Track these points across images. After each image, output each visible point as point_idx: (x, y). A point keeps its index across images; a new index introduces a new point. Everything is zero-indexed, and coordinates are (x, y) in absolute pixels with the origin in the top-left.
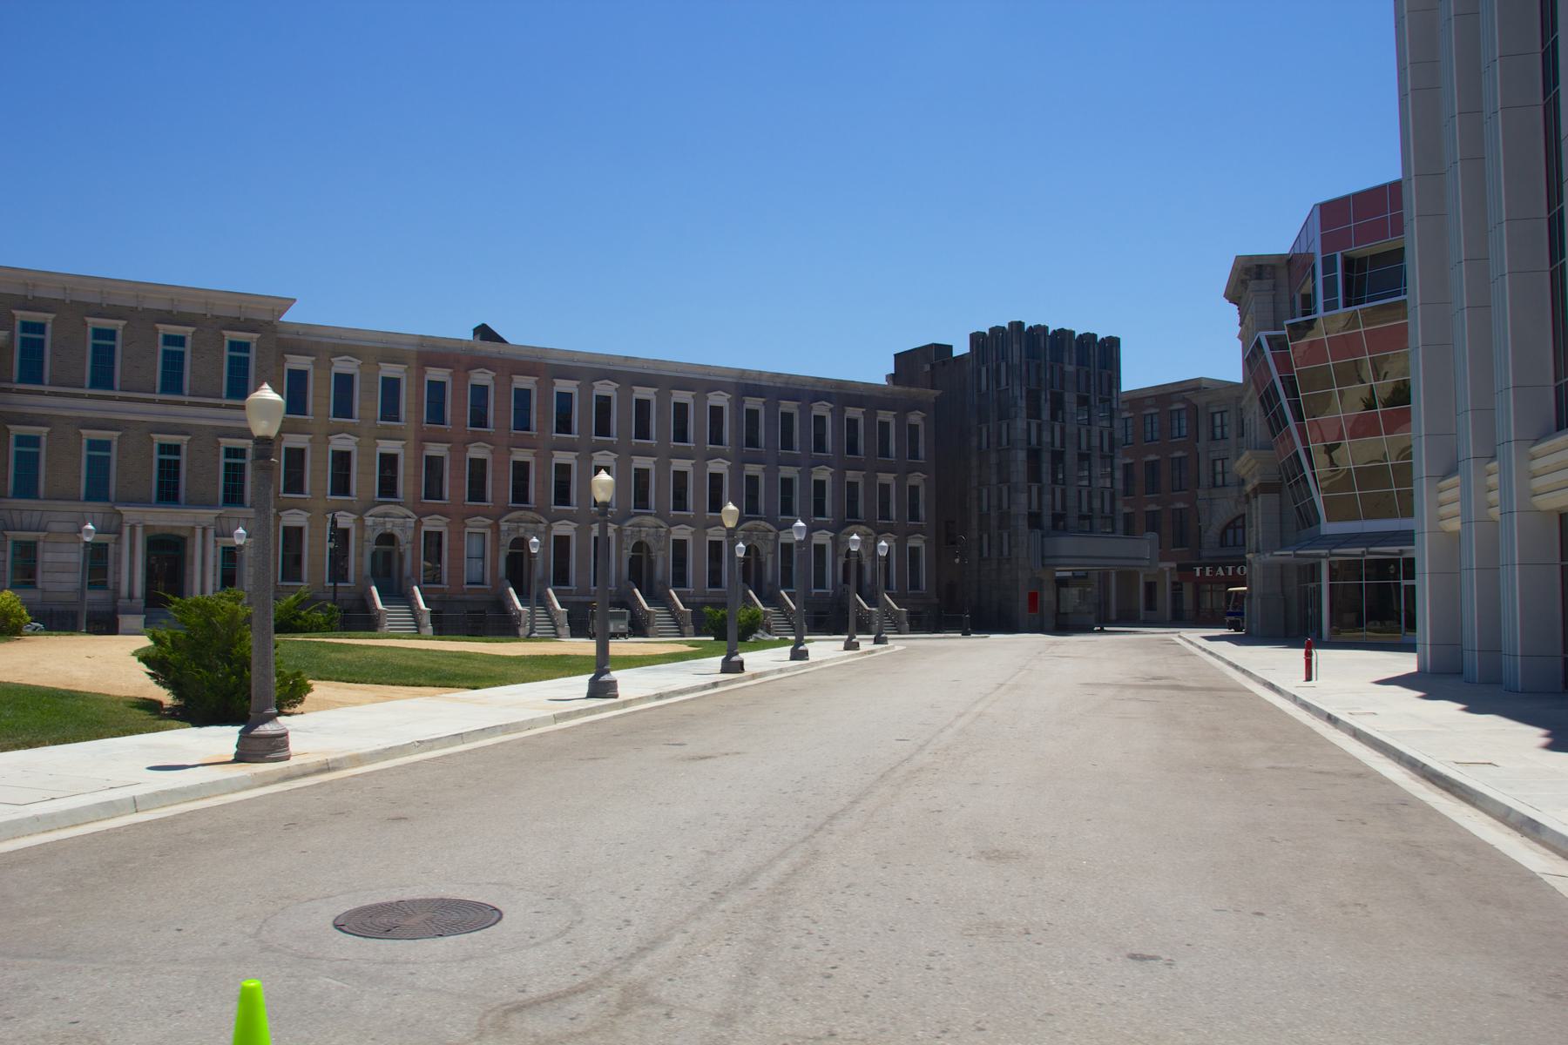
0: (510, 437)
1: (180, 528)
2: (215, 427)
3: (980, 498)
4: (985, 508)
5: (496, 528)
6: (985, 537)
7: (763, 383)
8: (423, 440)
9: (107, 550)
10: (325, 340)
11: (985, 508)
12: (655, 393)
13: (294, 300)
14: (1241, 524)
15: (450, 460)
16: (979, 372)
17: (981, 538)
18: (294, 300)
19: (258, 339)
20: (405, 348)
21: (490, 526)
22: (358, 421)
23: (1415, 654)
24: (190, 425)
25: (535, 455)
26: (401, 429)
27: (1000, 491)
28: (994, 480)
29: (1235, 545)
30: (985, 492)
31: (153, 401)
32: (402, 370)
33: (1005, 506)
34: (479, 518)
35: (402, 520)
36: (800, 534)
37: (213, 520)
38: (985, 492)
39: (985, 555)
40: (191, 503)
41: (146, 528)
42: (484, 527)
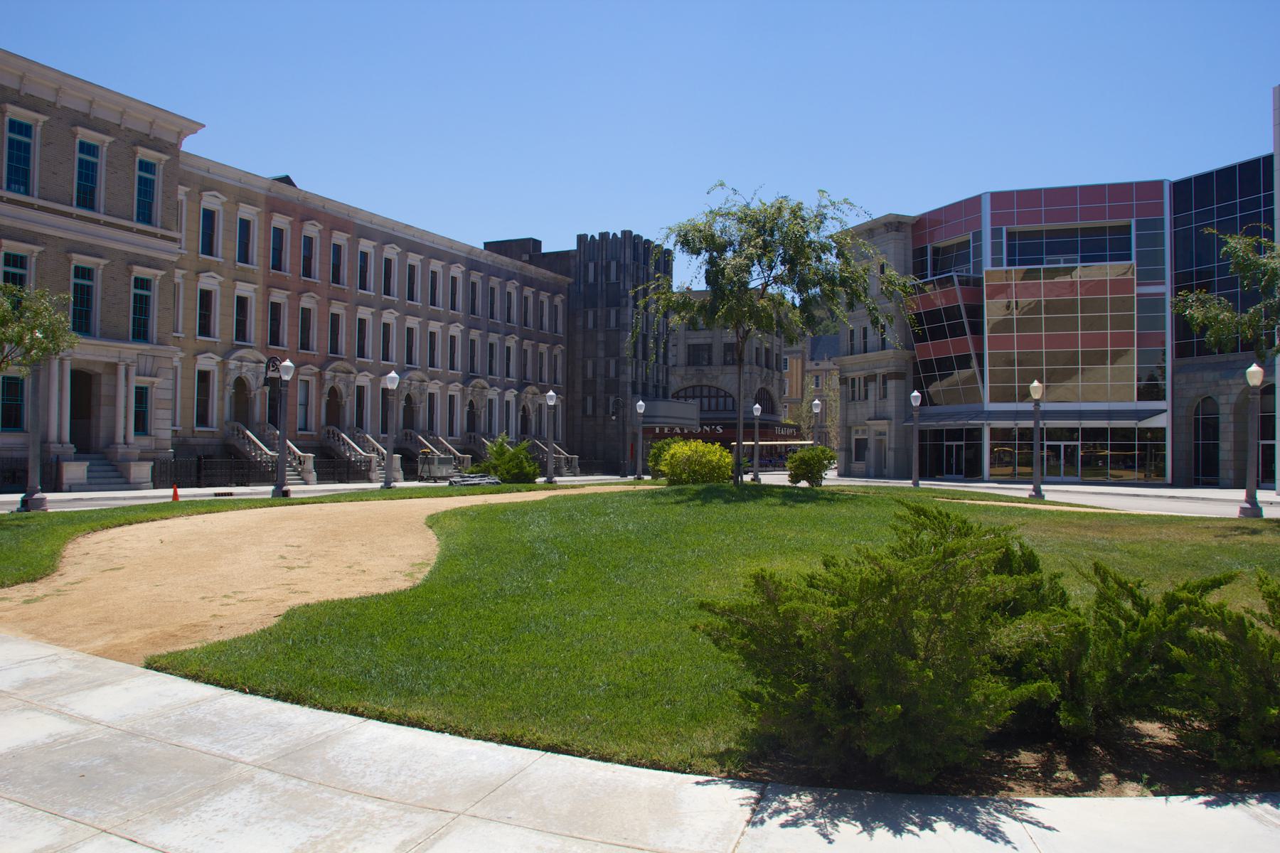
0: (329, 289)
1: (95, 362)
2: (126, 253)
3: (584, 367)
4: (590, 375)
5: (320, 376)
6: (590, 399)
7: (482, 260)
8: (269, 286)
9: (146, 393)
10: (195, 171)
11: (590, 375)
12: (421, 260)
13: (204, 126)
14: (683, 395)
15: (289, 307)
16: (586, 267)
17: (584, 399)
18: (204, 126)
19: (167, 161)
20: (258, 190)
21: (314, 374)
22: (222, 260)
23: (1244, 490)
24: (106, 248)
25: (346, 308)
26: (253, 273)
27: (608, 363)
28: (601, 354)
29: (717, 410)
30: (590, 364)
31: (69, 215)
32: (254, 212)
33: (612, 374)
34: (310, 366)
35: (254, 365)
36: (916, 401)
37: (135, 357)
38: (590, 364)
39: (589, 412)
40: (105, 336)
41: (73, 361)
42: (311, 375)
